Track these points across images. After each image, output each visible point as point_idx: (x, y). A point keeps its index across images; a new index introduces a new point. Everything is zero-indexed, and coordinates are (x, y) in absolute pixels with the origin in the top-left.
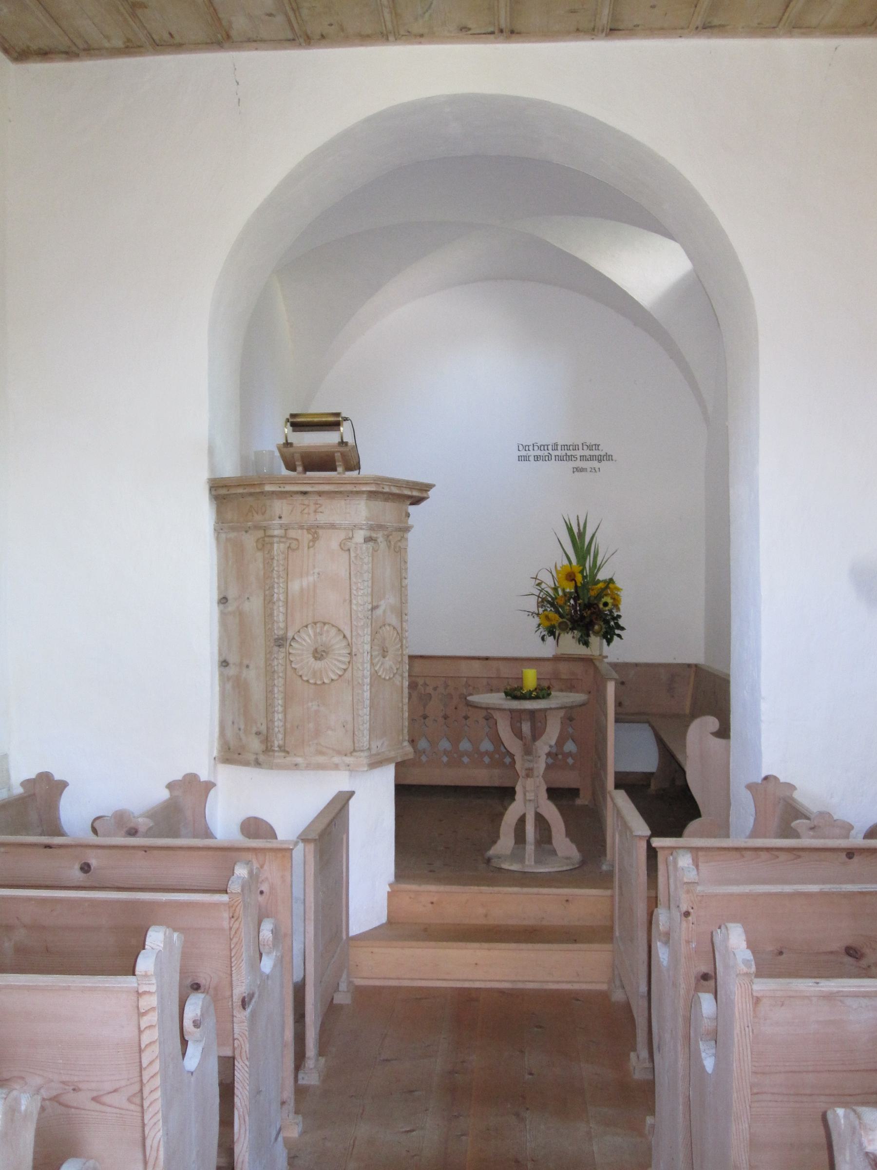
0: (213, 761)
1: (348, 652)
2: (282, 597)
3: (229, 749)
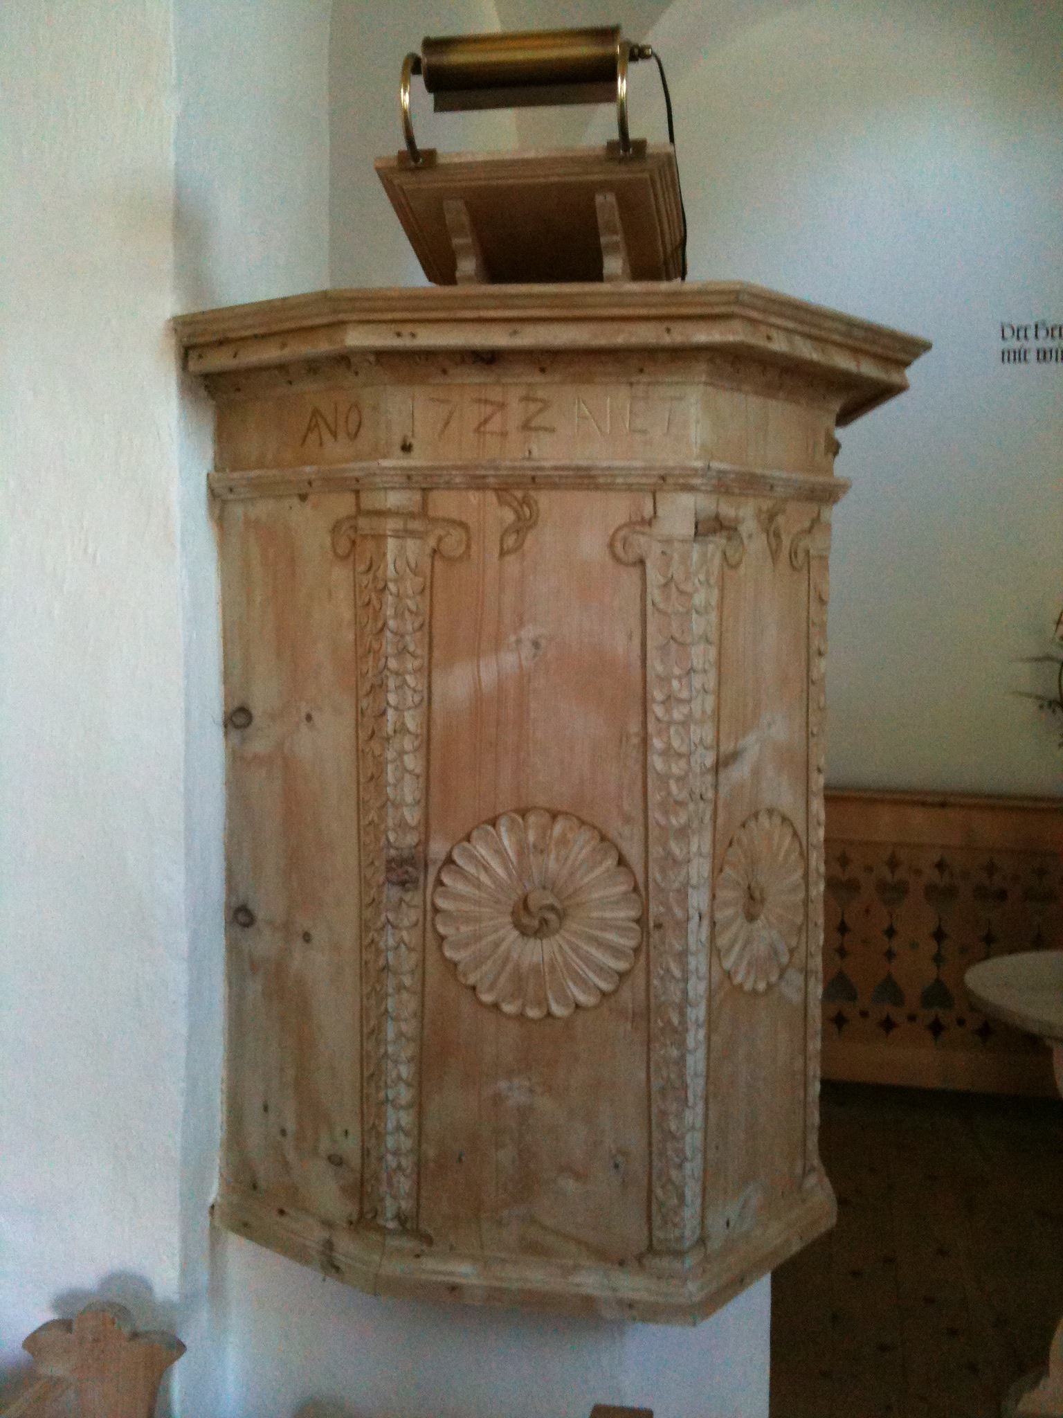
0: (205, 1220)
1: (633, 913)
2: (412, 722)
3: (255, 1187)
